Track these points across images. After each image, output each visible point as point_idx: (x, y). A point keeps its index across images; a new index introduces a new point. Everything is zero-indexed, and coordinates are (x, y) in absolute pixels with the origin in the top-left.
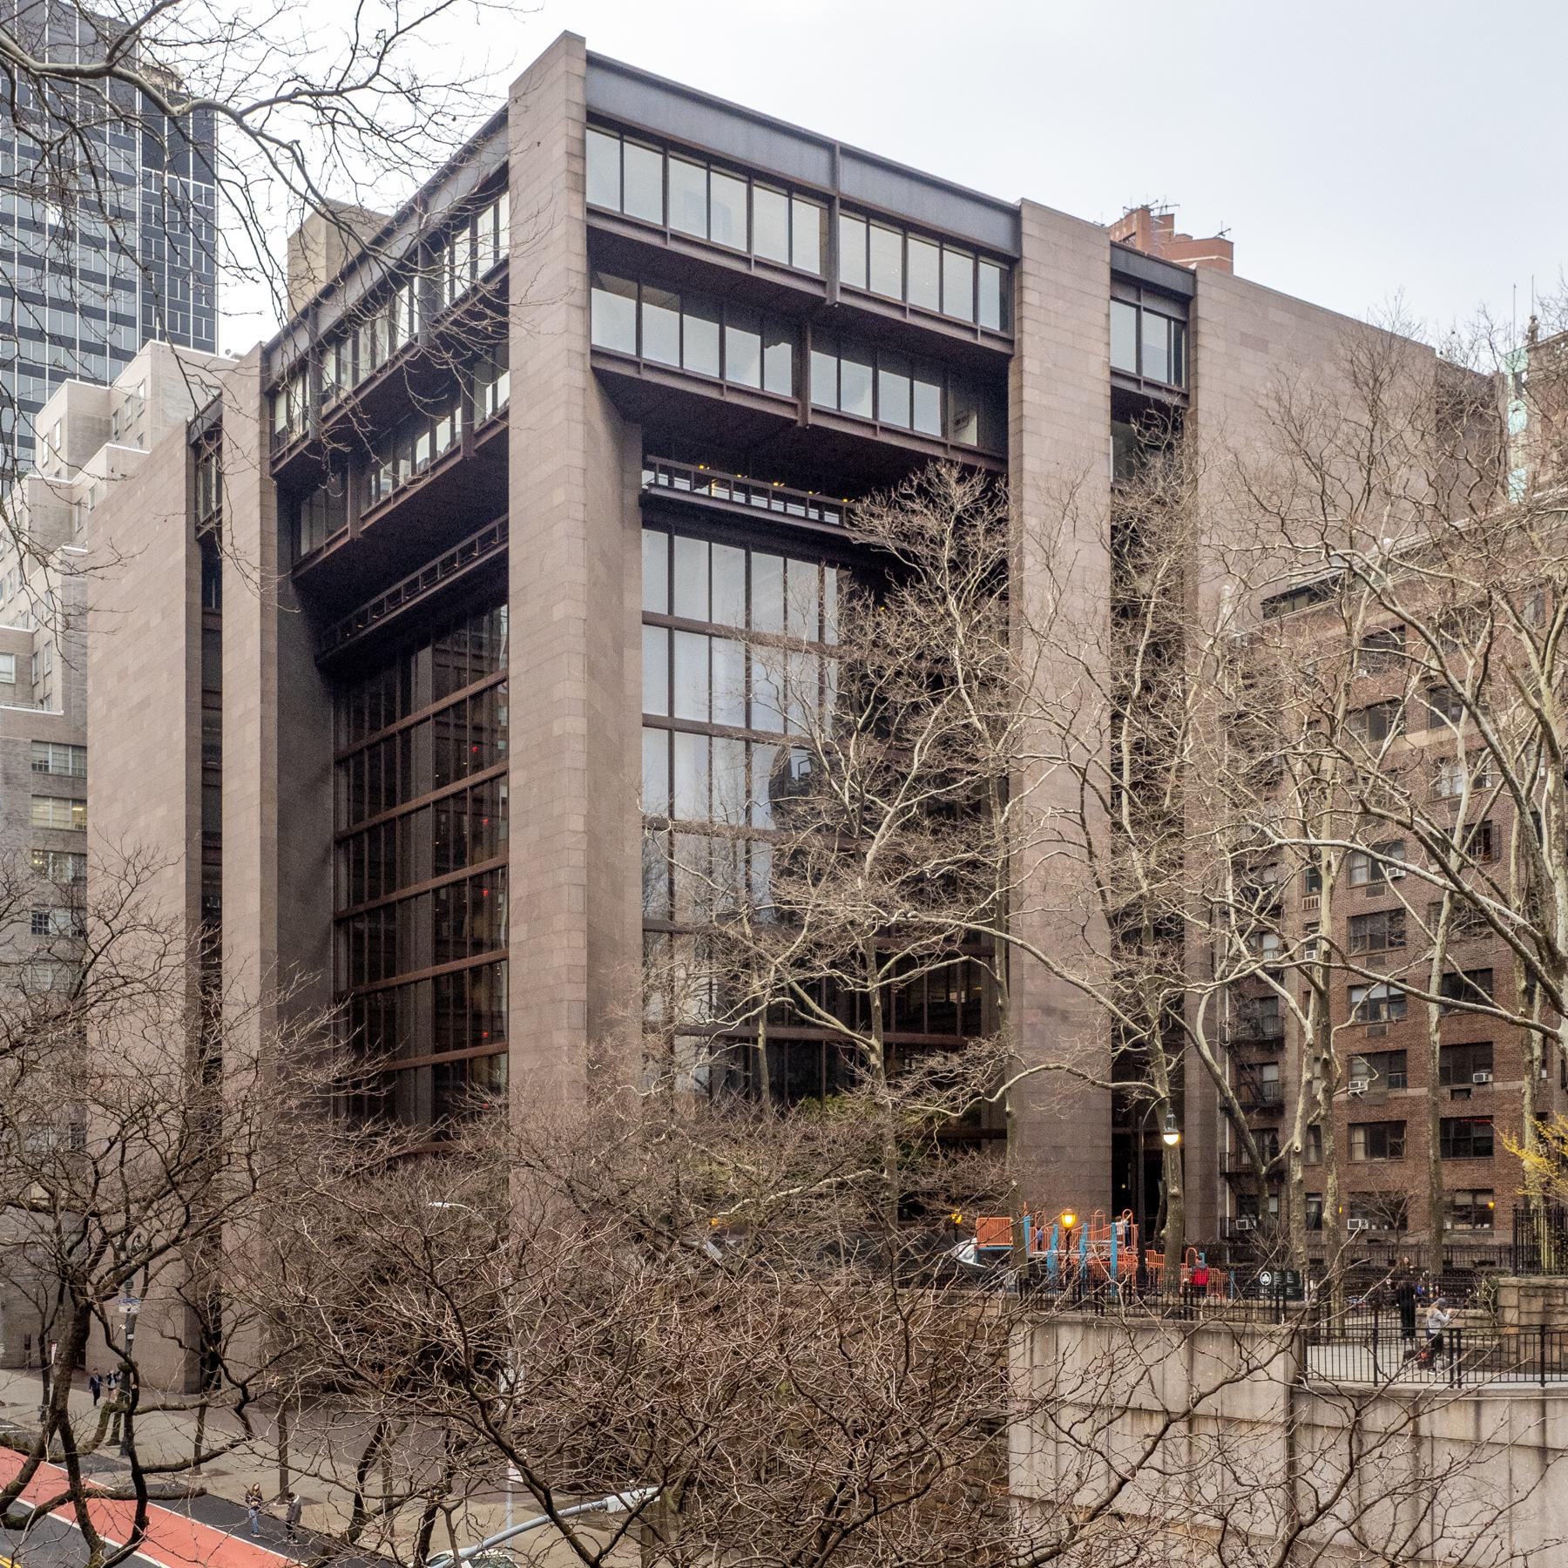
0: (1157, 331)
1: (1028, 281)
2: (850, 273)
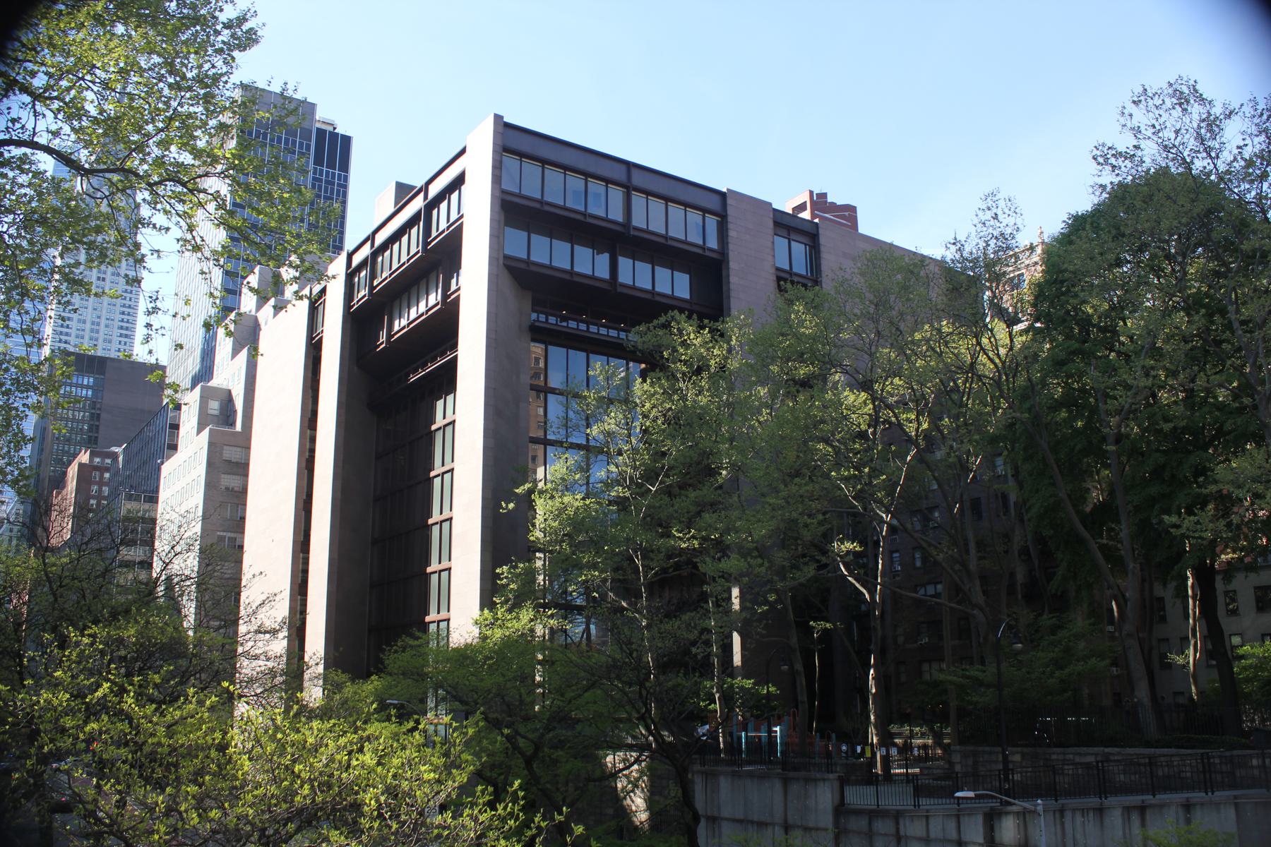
0: (799, 249)
1: (730, 226)
2: (638, 221)
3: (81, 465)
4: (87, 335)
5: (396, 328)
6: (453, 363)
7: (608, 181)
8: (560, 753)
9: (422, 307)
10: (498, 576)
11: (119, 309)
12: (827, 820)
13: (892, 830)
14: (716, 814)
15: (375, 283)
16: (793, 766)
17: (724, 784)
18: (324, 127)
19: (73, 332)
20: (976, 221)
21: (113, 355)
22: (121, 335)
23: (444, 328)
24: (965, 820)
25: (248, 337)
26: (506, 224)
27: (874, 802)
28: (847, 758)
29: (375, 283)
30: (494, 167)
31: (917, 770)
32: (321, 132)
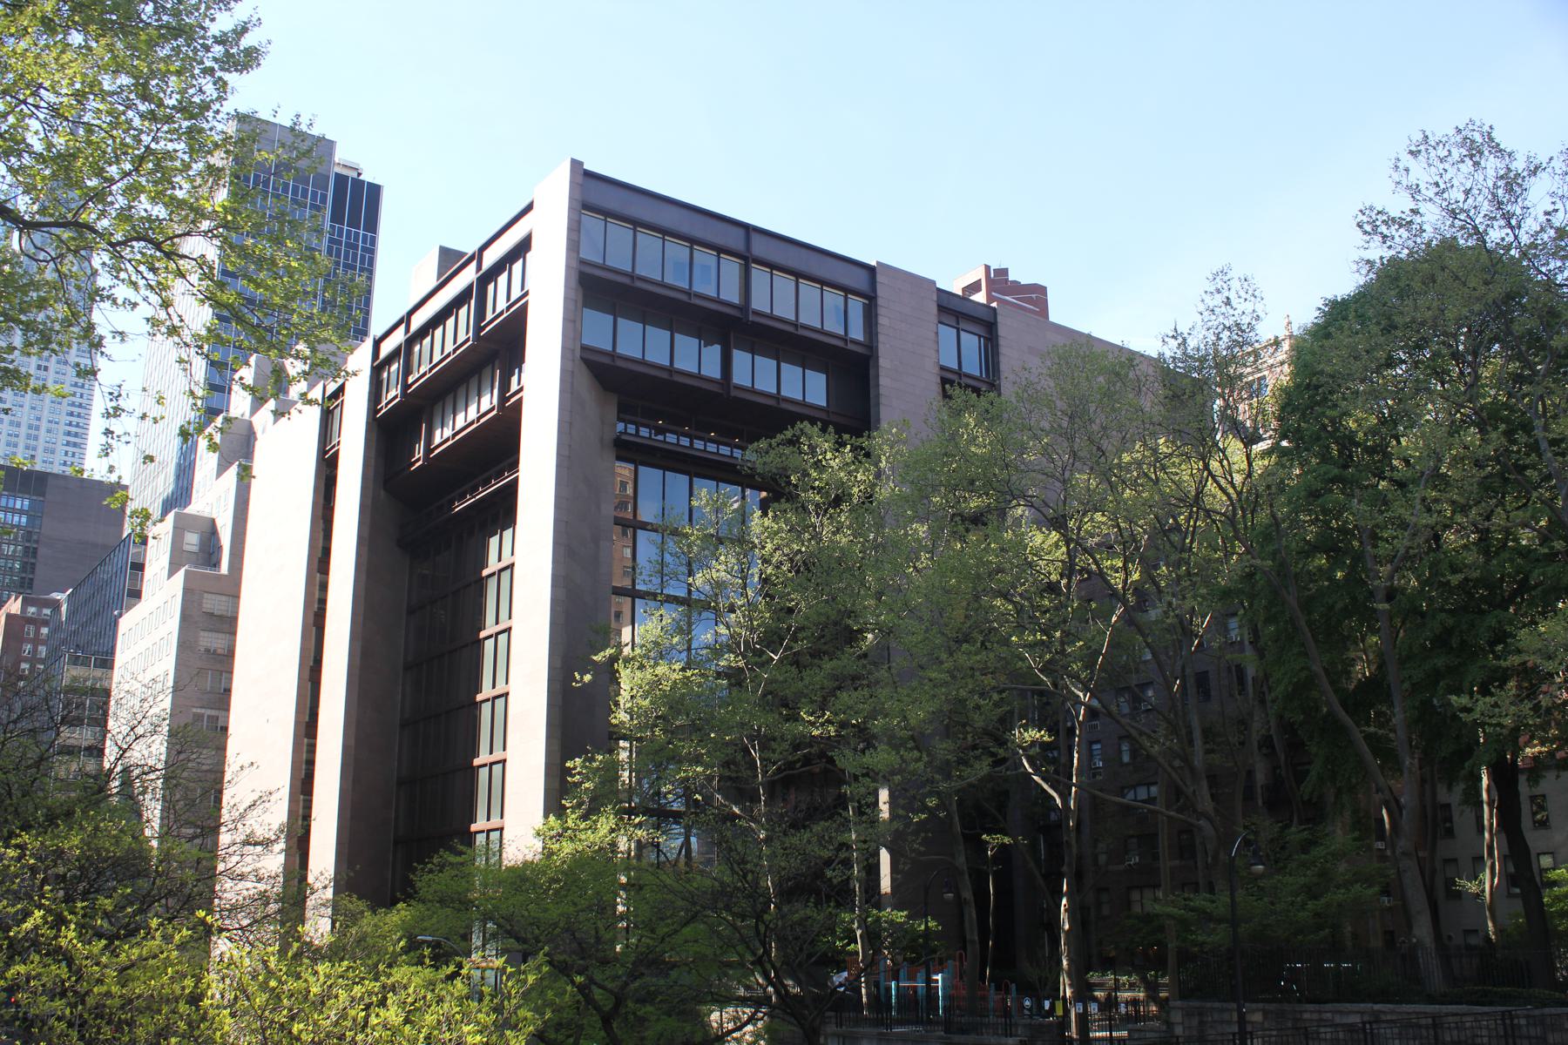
0: (971, 342)
1: (881, 311)
4: (22, 442)
5: (437, 440)
7: (720, 250)
10: (569, 772)
11: (66, 408)
15: (410, 380)
18: (345, 172)
21: (57, 469)
22: (68, 443)
23: (499, 443)
25: (239, 450)
26: (585, 305)
28: (1031, 1017)
29: (410, 380)
30: (570, 229)
31: (1125, 1033)
32: (341, 179)
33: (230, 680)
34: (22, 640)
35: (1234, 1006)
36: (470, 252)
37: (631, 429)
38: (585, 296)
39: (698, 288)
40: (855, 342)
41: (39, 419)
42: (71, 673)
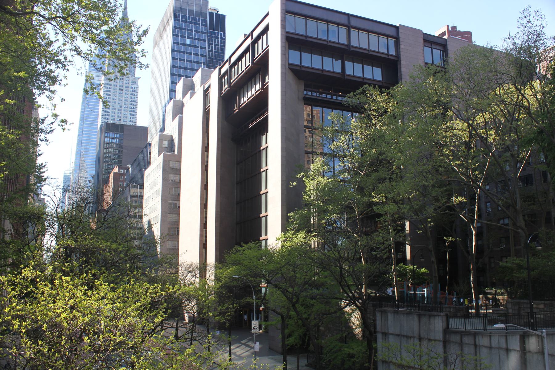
0: (437, 53)
1: (401, 43)
2: (354, 43)
3: (115, 173)
4: (116, 115)
5: (242, 102)
6: (267, 119)
7: (338, 24)
8: (314, 301)
9: (253, 91)
10: (289, 217)
11: (129, 103)
12: (440, 336)
13: (473, 342)
14: (386, 332)
15: (232, 81)
16: (425, 309)
17: (390, 317)
18: (213, 11)
19: (110, 114)
20: (518, 24)
21: (128, 123)
22: (131, 115)
23: (261, 102)
24: (510, 338)
25: (179, 110)
26: (290, 48)
27: (463, 327)
28: (456, 305)
29: (232, 81)
30: (282, 21)
31: (491, 311)
32: (211, 14)
33: (180, 190)
34: (119, 181)
35: (528, 301)
36: (248, 34)
37: (309, 93)
38: (289, 45)
39: (331, 39)
40: (391, 55)
41: (121, 107)
42: (132, 191)
